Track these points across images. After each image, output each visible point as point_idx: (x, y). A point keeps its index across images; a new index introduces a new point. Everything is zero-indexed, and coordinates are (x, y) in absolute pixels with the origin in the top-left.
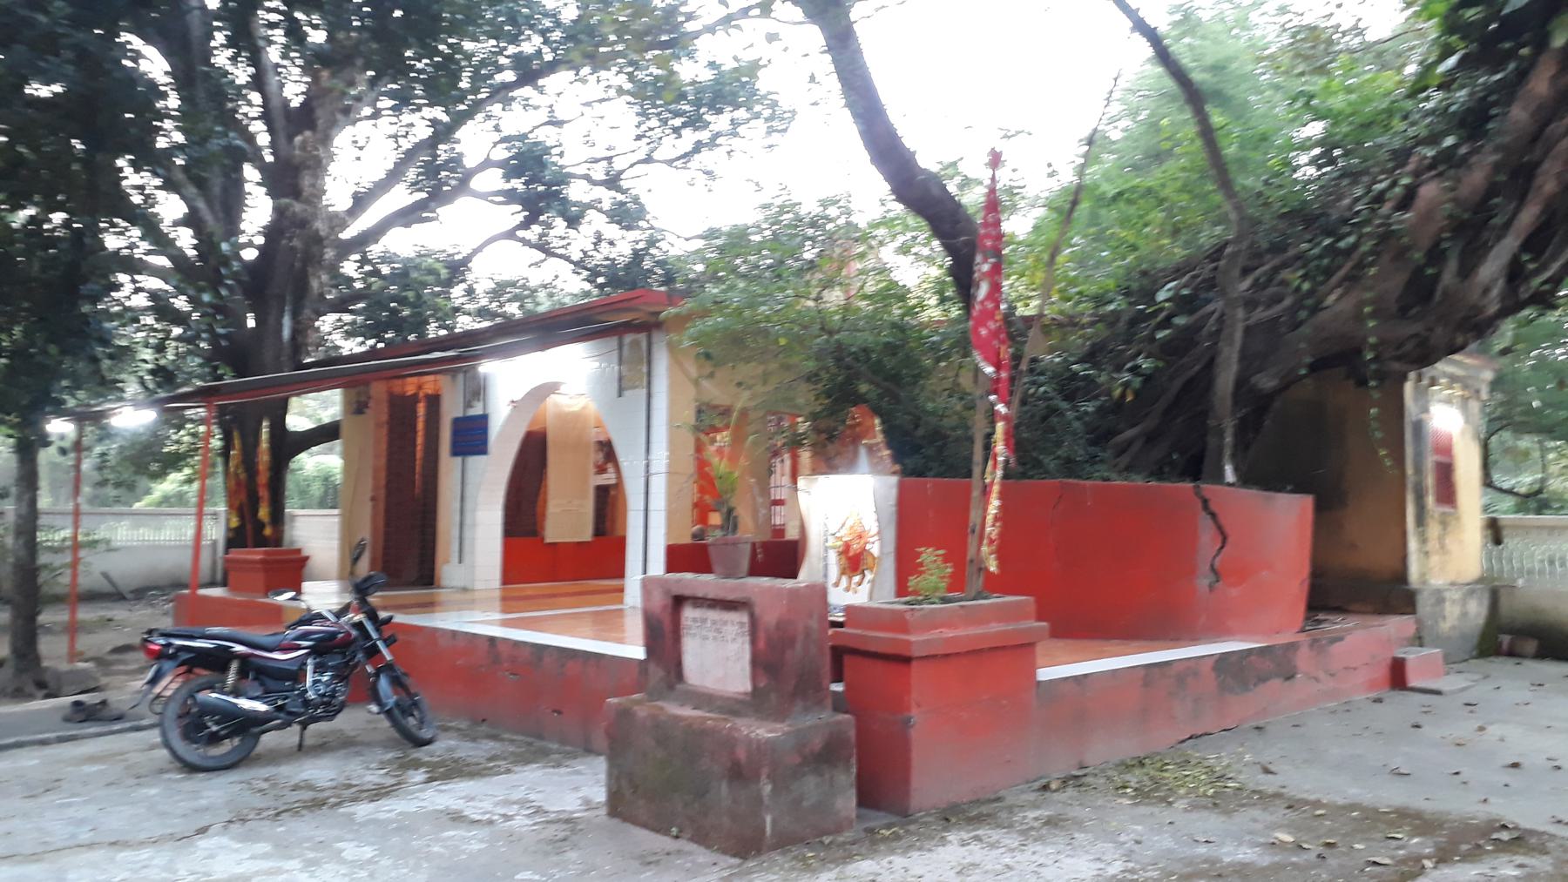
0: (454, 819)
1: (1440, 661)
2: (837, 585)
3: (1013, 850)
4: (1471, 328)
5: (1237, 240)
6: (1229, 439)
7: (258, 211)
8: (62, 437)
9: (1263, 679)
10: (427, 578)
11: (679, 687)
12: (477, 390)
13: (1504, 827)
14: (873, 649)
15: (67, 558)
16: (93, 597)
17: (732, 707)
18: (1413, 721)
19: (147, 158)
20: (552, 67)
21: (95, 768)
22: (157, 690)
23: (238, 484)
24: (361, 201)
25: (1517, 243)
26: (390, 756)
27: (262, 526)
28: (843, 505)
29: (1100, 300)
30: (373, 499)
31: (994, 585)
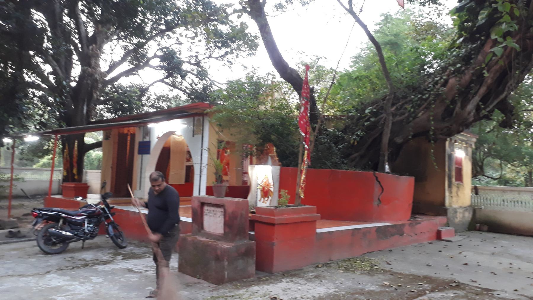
0: (129, 271)
1: (454, 232)
3: (301, 284)
4: (464, 125)
5: (390, 94)
6: (386, 158)
7: (76, 71)
8: (8, 144)
9: (392, 235)
11: (202, 231)
12: (147, 133)
13: (455, 282)
15: (8, 184)
16: (17, 197)
17: (218, 238)
18: (439, 250)
19: (41, 52)
20: (177, 25)
21: (16, 252)
22: (36, 227)
23: (67, 161)
24: (112, 67)
25: (479, 99)
26: (112, 251)
27: (74, 175)
28: (262, 174)
29: (348, 111)
30: (112, 168)
31: (304, 202)
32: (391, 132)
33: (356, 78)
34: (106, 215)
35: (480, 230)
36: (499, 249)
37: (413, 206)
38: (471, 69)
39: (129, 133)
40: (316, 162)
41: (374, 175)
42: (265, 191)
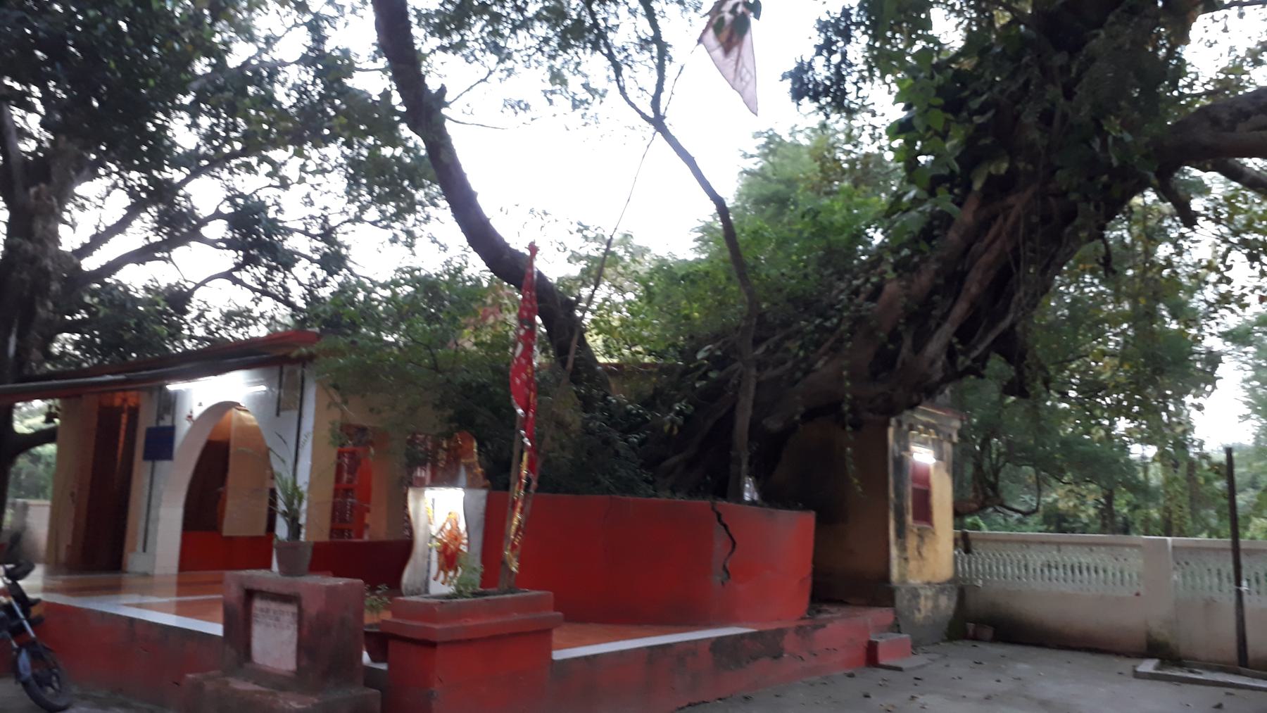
4: (925, 391)
6: (744, 467)
9: (755, 658)
10: (115, 563)
11: (246, 665)
12: (170, 404)
14: (408, 635)
24: (98, 240)
25: (954, 329)
31: (522, 581)
32: (754, 407)
34: (14, 623)
35: (976, 638)
39: (126, 406)
40: (548, 482)
41: (713, 509)
42: (449, 552)
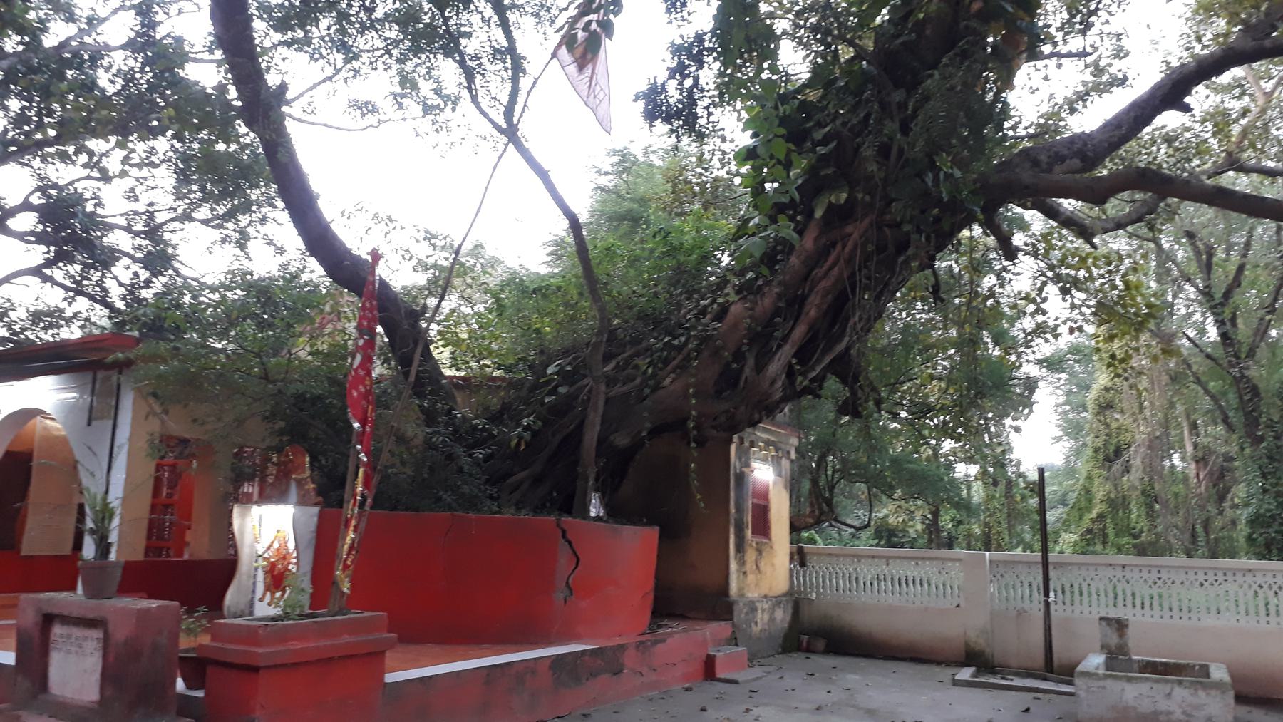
2: (261, 600)
4: (767, 410)
9: (593, 674)
11: (41, 697)
14: (229, 660)
31: (355, 601)
33: (534, 291)
35: (809, 650)
36: (837, 695)
37: (656, 598)
38: (774, 283)
40: (385, 497)
